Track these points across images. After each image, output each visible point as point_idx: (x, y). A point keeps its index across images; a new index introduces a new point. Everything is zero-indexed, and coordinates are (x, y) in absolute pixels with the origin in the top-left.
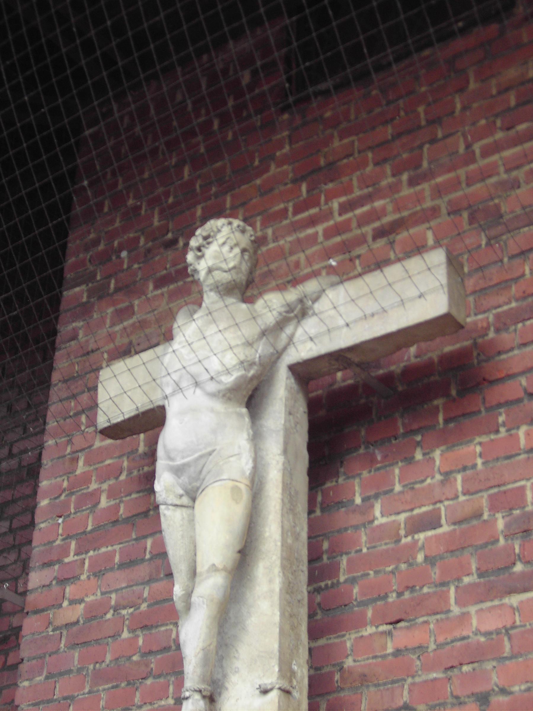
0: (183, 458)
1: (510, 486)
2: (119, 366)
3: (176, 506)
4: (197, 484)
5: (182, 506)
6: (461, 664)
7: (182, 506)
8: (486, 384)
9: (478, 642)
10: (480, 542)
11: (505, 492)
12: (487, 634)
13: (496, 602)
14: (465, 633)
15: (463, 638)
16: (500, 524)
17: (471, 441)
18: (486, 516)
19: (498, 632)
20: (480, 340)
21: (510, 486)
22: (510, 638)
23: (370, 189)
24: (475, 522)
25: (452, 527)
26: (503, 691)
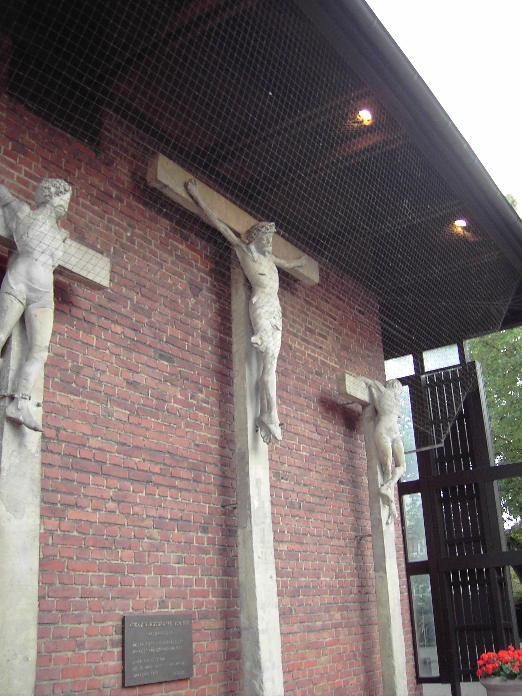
0: (40, 287)
1: (74, 352)
2: (108, 268)
3: (20, 302)
4: (37, 300)
5: (22, 303)
6: (52, 413)
7: (22, 303)
8: (71, 304)
9: (58, 407)
10: (63, 368)
11: (73, 353)
12: (62, 405)
13: (66, 394)
14: (54, 401)
15: (53, 403)
16: (70, 365)
17: (64, 324)
18: (65, 358)
19: (65, 406)
20: (72, 284)
21: (74, 352)
22: (69, 410)
23: (39, 176)
24: (61, 358)
25: (53, 355)
26: (65, 429)
